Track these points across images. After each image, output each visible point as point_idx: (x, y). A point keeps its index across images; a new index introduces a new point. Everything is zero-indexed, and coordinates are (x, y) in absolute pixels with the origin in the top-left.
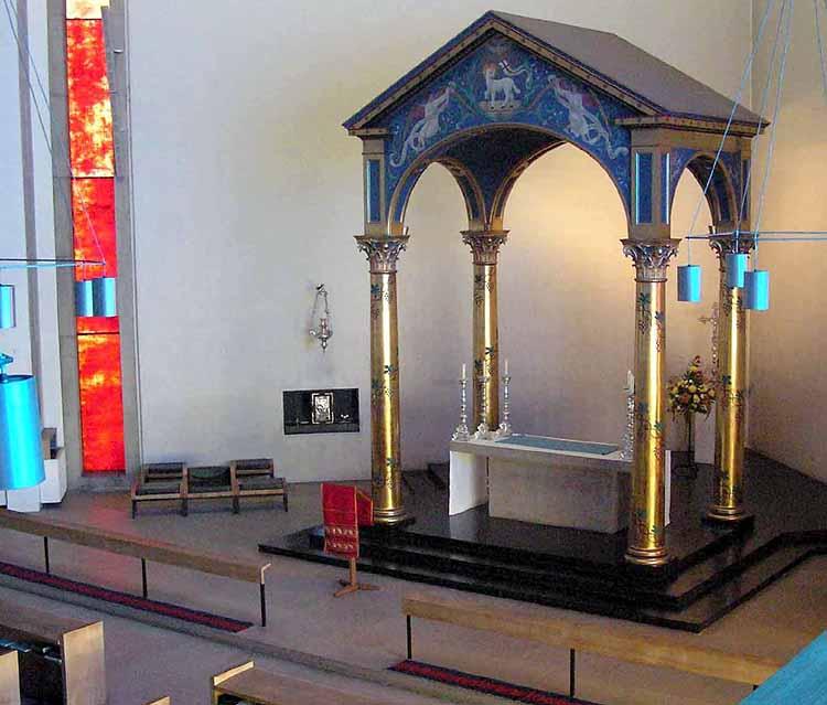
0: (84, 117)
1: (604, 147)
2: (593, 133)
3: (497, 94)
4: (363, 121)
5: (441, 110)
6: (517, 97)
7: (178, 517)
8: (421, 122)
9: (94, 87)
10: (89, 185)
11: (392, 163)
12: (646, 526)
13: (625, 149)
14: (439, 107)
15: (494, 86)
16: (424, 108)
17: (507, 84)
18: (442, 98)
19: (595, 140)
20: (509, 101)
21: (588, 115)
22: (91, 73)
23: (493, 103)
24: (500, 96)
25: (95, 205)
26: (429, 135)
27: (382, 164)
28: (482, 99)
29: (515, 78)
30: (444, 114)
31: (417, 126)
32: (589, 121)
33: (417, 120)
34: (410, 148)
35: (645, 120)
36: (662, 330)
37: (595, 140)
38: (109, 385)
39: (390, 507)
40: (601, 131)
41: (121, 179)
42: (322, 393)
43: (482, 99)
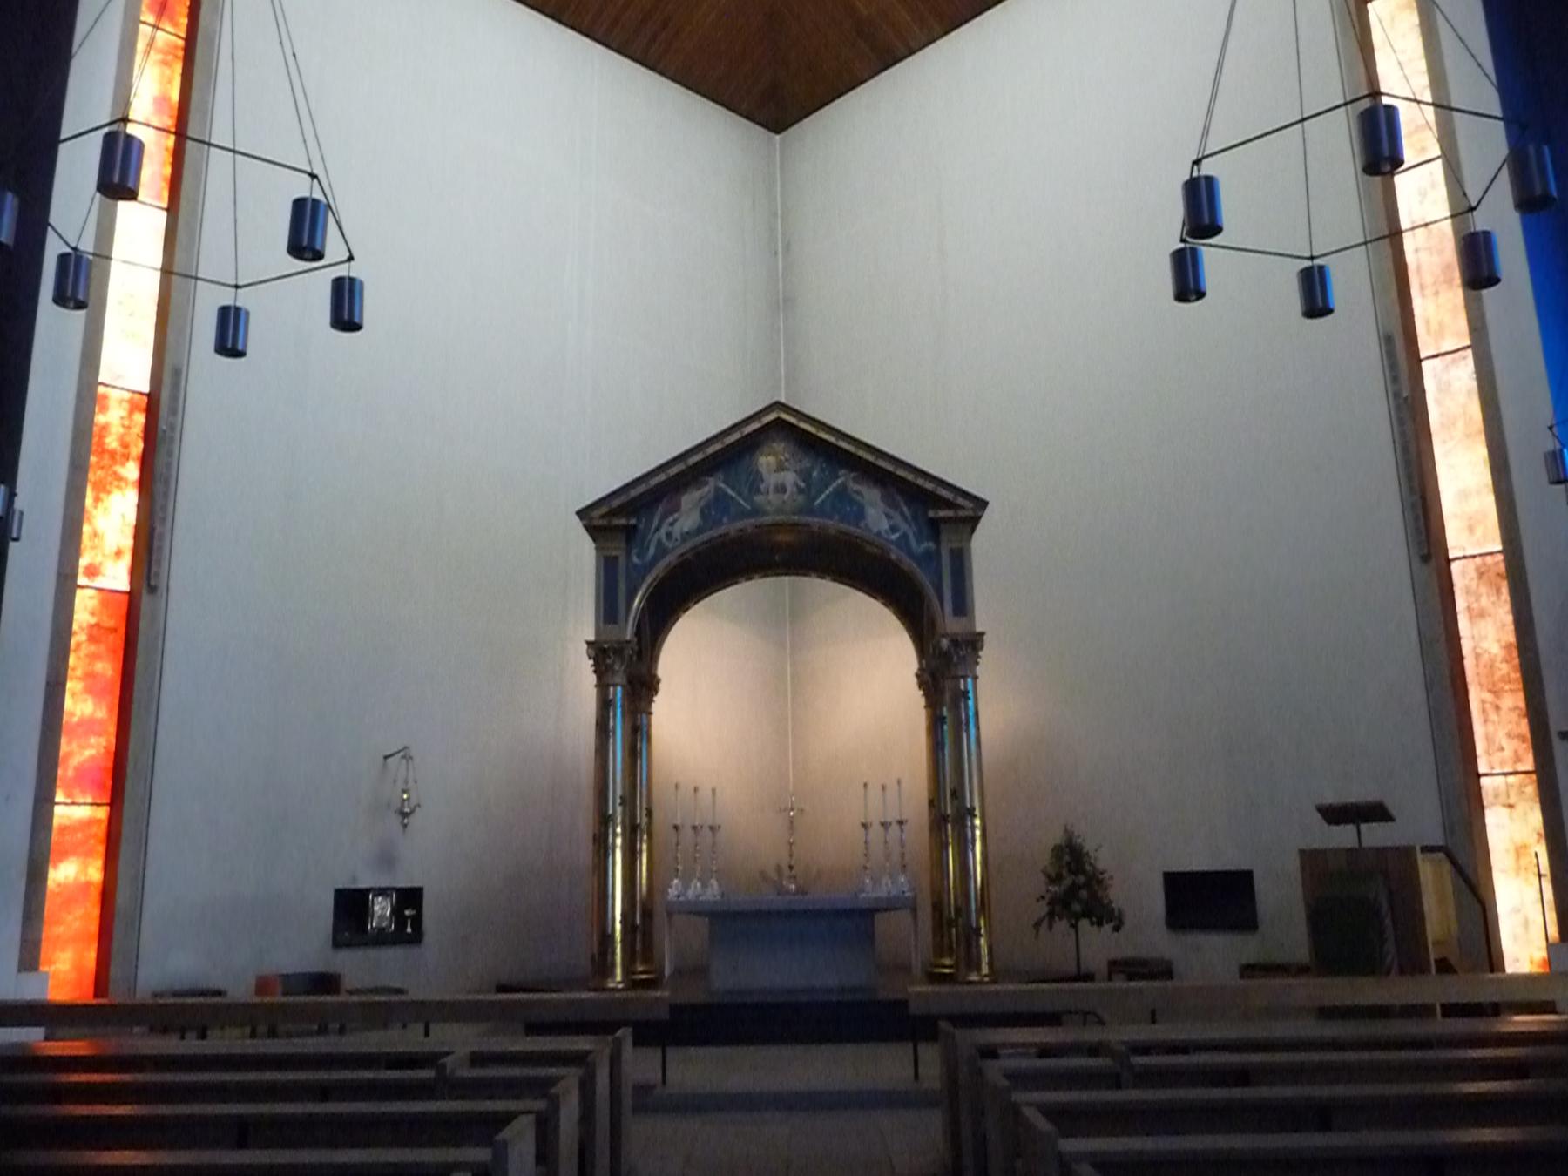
0: (96, 507)
2: (893, 529)
4: (604, 510)
5: (702, 503)
6: (800, 491)
7: (978, 681)
8: (676, 515)
9: (115, 473)
10: (91, 598)
11: (635, 560)
12: (971, 910)
13: (931, 545)
14: (701, 498)
15: (771, 479)
17: (789, 478)
18: (706, 489)
19: (897, 535)
20: (792, 493)
22: (113, 454)
23: (771, 497)
24: (781, 489)
25: (97, 625)
26: (686, 529)
27: (622, 561)
28: (758, 491)
29: (799, 473)
30: (707, 506)
31: (671, 519)
32: (888, 516)
33: (671, 512)
34: (659, 542)
35: (961, 513)
37: (897, 535)
38: (83, 879)
39: (619, 978)
40: (904, 527)
41: (153, 590)
42: (382, 892)
43: (758, 491)
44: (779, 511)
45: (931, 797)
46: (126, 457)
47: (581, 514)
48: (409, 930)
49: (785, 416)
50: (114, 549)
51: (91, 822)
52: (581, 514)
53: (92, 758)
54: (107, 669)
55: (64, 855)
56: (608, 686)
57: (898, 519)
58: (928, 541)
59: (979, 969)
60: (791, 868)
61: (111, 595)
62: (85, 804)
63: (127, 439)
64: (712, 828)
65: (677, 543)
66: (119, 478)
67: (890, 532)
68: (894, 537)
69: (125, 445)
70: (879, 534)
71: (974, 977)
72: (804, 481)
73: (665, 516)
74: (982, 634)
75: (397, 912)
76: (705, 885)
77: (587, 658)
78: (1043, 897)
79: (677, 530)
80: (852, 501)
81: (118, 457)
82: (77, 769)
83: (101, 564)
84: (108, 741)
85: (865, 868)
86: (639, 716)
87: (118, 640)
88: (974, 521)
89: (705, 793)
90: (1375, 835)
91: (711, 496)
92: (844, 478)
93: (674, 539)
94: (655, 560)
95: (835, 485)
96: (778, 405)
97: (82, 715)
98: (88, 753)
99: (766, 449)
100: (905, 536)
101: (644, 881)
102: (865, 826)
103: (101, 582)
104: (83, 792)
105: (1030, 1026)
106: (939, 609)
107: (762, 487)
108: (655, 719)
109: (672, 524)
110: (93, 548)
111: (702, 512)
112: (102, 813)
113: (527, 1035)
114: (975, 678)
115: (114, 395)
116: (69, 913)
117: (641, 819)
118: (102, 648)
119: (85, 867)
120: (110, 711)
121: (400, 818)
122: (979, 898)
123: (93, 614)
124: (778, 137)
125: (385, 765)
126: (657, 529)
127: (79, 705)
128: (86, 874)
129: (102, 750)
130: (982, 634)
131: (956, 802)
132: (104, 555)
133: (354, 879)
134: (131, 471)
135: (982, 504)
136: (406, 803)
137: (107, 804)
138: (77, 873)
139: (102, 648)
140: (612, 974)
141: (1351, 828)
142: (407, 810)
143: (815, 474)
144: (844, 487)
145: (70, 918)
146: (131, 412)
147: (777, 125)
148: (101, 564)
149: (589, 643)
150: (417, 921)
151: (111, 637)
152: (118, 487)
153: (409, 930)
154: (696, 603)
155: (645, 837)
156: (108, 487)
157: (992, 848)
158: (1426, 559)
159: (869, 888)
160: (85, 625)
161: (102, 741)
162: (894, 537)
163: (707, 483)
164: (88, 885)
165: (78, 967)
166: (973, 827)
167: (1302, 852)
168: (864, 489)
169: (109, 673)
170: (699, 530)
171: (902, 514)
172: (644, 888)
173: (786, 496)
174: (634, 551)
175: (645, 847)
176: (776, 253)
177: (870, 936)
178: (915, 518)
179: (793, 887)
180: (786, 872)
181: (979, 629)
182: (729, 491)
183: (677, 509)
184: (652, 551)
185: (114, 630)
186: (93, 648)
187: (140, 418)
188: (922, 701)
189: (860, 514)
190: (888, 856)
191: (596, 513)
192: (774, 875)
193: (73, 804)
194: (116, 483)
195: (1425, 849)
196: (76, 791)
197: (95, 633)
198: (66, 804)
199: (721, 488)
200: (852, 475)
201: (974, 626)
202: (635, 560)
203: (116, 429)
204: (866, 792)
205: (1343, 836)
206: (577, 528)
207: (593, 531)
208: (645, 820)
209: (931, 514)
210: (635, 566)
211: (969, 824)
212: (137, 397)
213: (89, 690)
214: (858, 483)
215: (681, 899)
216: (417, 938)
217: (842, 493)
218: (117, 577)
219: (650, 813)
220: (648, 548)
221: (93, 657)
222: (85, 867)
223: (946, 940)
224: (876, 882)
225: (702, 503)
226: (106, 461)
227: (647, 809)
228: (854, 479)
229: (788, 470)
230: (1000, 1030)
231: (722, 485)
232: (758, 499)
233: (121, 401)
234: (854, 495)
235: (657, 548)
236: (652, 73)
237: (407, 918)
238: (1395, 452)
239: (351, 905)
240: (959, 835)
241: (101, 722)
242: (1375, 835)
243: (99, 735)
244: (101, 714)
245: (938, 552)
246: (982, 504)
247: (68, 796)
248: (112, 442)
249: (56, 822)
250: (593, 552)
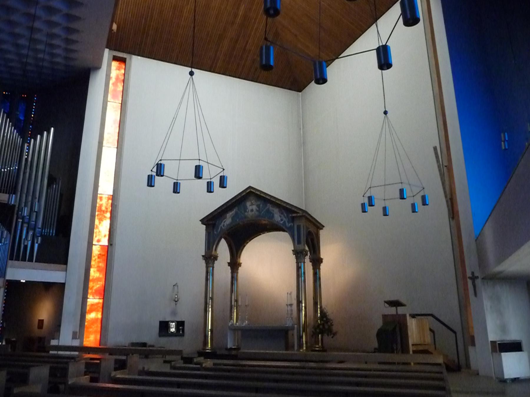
0: (99, 225)
2: (282, 220)
6: (257, 211)
10: (98, 247)
11: (215, 232)
13: (292, 224)
17: (254, 207)
18: (233, 212)
19: (283, 222)
22: (104, 211)
25: (100, 254)
30: (233, 217)
32: (280, 216)
34: (221, 227)
37: (283, 222)
38: (96, 317)
39: (209, 347)
40: (284, 219)
46: (107, 212)
48: (181, 332)
49: (252, 190)
50: (104, 235)
51: (99, 303)
53: (99, 287)
54: (102, 265)
55: (91, 311)
56: (209, 267)
61: (103, 247)
62: (97, 299)
63: (107, 207)
66: (105, 217)
69: (107, 209)
72: (258, 208)
75: (177, 328)
81: (105, 212)
82: (95, 290)
83: (101, 239)
84: (103, 283)
86: (234, 274)
87: (105, 258)
90: (401, 310)
92: (269, 206)
97: (96, 276)
98: (98, 286)
100: (285, 222)
103: (101, 243)
104: (97, 296)
105: (213, 359)
107: (247, 211)
109: (225, 222)
110: (99, 235)
111: (232, 218)
112: (101, 301)
113: (181, 360)
115: (104, 196)
116: (94, 325)
118: (101, 260)
119: (97, 314)
120: (103, 275)
121: (175, 302)
123: (99, 251)
125: (174, 288)
127: (94, 273)
128: (97, 316)
129: (101, 285)
132: (102, 237)
133: (165, 319)
134: (108, 215)
136: (176, 298)
137: (102, 299)
138: (95, 316)
139: (101, 260)
140: (208, 346)
141: (394, 308)
142: (176, 300)
143: (261, 206)
145: (93, 327)
146: (108, 200)
147: (300, 90)
148: (101, 239)
149: (203, 256)
150: (183, 330)
151: (103, 257)
152: (105, 219)
153: (181, 332)
154: (250, 241)
155: (235, 308)
156: (103, 220)
157: (214, 314)
158: (453, 218)
160: (97, 255)
161: (101, 283)
162: (282, 222)
164: (98, 319)
165: (96, 339)
166: (302, 306)
167: (383, 315)
168: (274, 209)
169: (103, 266)
171: (284, 215)
173: (253, 213)
174: (215, 230)
176: (300, 129)
178: (288, 216)
183: (226, 218)
185: (104, 255)
186: (99, 260)
187: (110, 201)
193: (94, 298)
194: (104, 218)
195: (413, 316)
196: (95, 296)
197: (100, 256)
198: (92, 299)
203: (104, 205)
205: (392, 311)
212: (110, 196)
213: (98, 271)
216: (183, 335)
218: (105, 242)
221: (99, 262)
222: (97, 314)
225: (232, 215)
226: (102, 213)
228: (272, 206)
229: (254, 205)
230: (248, 361)
232: (246, 213)
233: (106, 198)
235: (220, 229)
236: (256, 83)
237: (180, 329)
238: (115, 249)
239: (164, 326)
241: (101, 278)
242: (401, 310)
243: (100, 281)
244: (101, 276)
245: (294, 225)
247: (93, 296)
248: (103, 208)
249: (88, 304)
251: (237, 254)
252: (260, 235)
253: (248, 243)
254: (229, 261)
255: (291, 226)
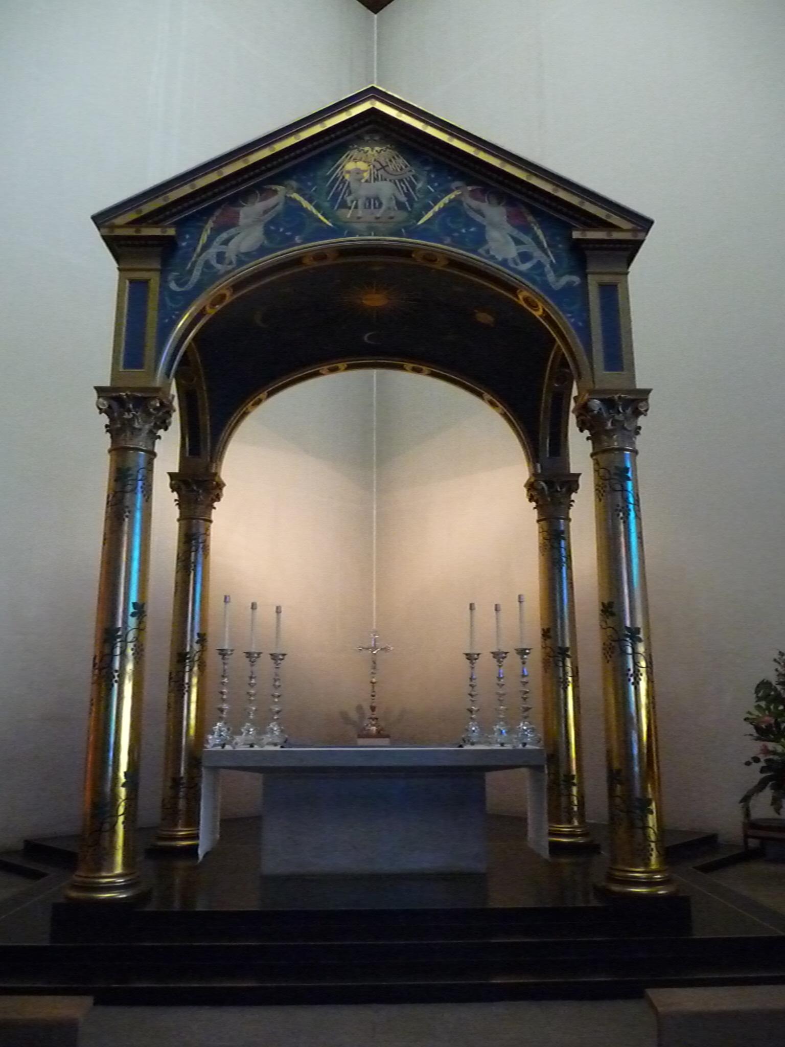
1: (543, 274)
2: (525, 257)
3: (368, 199)
4: (132, 216)
5: (268, 217)
6: (401, 206)
8: (233, 231)
11: (173, 286)
13: (576, 279)
14: (265, 212)
16: (238, 214)
17: (386, 189)
18: (272, 201)
21: (516, 233)
24: (374, 202)
26: (244, 248)
28: (344, 205)
30: (272, 222)
31: (224, 236)
32: (518, 242)
34: (207, 265)
35: (616, 235)
36: (650, 681)
39: (119, 870)
40: (538, 254)
44: (371, 229)
45: (546, 627)
47: (100, 219)
52: (100, 219)
57: (529, 246)
58: (571, 273)
59: (646, 862)
60: (373, 709)
64: (274, 657)
65: (230, 267)
67: (518, 261)
68: (525, 267)
70: (504, 263)
71: (639, 873)
73: (216, 231)
74: (647, 392)
76: (261, 731)
77: (170, 490)
78: (756, 760)
79: (231, 251)
80: (470, 222)
85: (471, 711)
88: (631, 249)
89: (265, 614)
91: (280, 208)
93: (227, 261)
94: (199, 288)
95: (446, 200)
96: (373, 93)
99: (355, 153)
100: (539, 265)
101: (193, 722)
102: (471, 657)
106: (585, 358)
108: (214, 529)
109: (226, 242)
114: (635, 452)
117: (191, 646)
122: (645, 760)
124: (376, 16)
126: (206, 247)
130: (647, 392)
131: (548, 642)
135: (645, 224)
140: (111, 867)
144: (457, 201)
149: (100, 390)
155: (196, 669)
159: (475, 737)
163: (275, 192)
168: (485, 206)
170: (262, 251)
171: (536, 239)
172: (192, 732)
173: (379, 213)
175: (195, 680)
177: (481, 799)
179: (374, 728)
180: (368, 713)
181: (640, 384)
182: (305, 204)
183: (231, 223)
184: (196, 275)
188: (535, 514)
189: (480, 239)
190: (501, 698)
191: (120, 220)
192: (354, 715)
199: (294, 200)
200: (470, 188)
201: (633, 377)
202: (173, 286)
204: (471, 614)
206: (94, 235)
207: (115, 244)
208: (132, 622)
209: (576, 235)
210: (173, 294)
211: (630, 650)
214: (477, 199)
215: (228, 747)
217: (453, 210)
219: (202, 638)
220: (190, 272)
223: (564, 800)
224: (486, 729)
227: (199, 635)
228: (473, 194)
231: (296, 196)
234: (472, 214)
240: (615, 669)
245: (584, 284)
246: (645, 224)
250: (116, 274)
251: (215, 441)
252: (317, 374)
253: (259, 402)
254: (176, 469)
255: (569, 287)
